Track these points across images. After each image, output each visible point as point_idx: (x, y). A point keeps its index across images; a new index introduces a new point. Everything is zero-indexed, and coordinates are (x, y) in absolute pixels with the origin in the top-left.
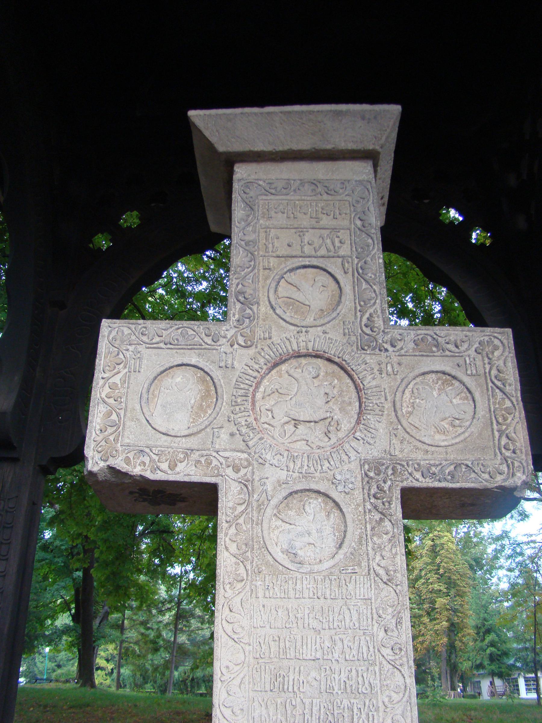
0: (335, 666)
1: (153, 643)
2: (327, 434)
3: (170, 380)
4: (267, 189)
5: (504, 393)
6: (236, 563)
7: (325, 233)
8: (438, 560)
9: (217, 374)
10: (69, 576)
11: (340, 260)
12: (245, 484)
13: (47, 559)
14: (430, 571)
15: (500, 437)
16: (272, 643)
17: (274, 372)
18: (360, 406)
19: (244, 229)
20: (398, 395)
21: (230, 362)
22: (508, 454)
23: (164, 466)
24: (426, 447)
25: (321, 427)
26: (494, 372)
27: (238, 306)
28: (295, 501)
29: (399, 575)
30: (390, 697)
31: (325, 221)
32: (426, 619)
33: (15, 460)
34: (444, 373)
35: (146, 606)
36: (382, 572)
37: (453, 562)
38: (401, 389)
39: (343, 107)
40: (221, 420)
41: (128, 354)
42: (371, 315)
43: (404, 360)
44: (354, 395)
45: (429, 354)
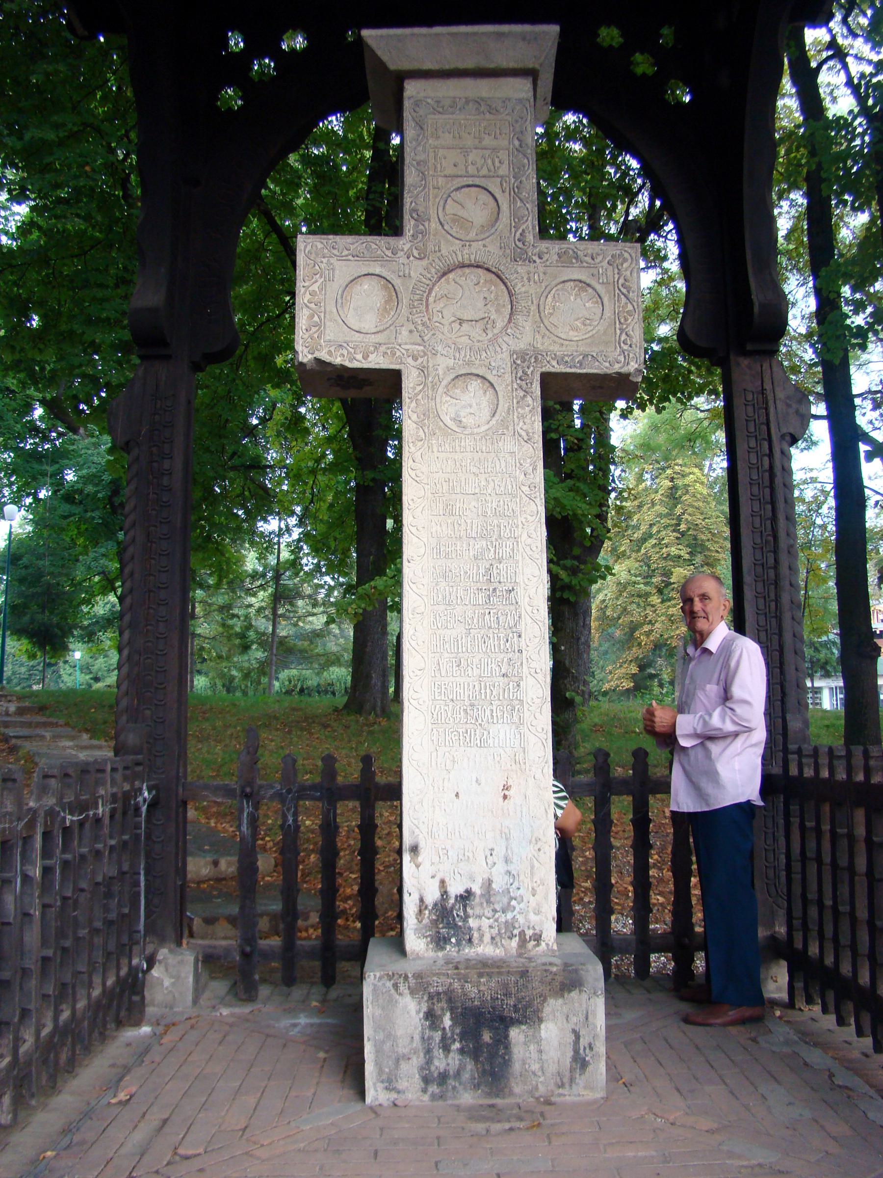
0: (488, 498)
1: (241, 638)
2: (485, 330)
3: (359, 287)
4: (435, 107)
5: (628, 299)
6: (417, 428)
7: (487, 153)
8: (678, 510)
9: (397, 282)
10: (110, 539)
11: (499, 180)
12: (422, 369)
13: (75, 514)
14: (665, 527)
15: (621, 334)
16: (444, 483)
17: (443, 279)
18: (512, 308)
19: (415, 148)
20: (542, 299)
21: (407, 272)
22: (625, 347)
23: (359, 357)
24: (562, 341)
25: (481, 325)
26: (621, 281)
27: (413, 222)
28: (460, 382)
29: (536, 436)
30: (526, 518)
31: (488, 141)
32: (655, 599)
33: (167, 357)
34: (580, 281)
35: (228, 583)
36: (523, 434)
37: (702, 514)
38: (545, 295)
39: (505, 28)
40: (402, 320)
41: (322, 266)
42: (523, 230)
43: (549, 270)
44: (507, 298)
45: (570, 265)
